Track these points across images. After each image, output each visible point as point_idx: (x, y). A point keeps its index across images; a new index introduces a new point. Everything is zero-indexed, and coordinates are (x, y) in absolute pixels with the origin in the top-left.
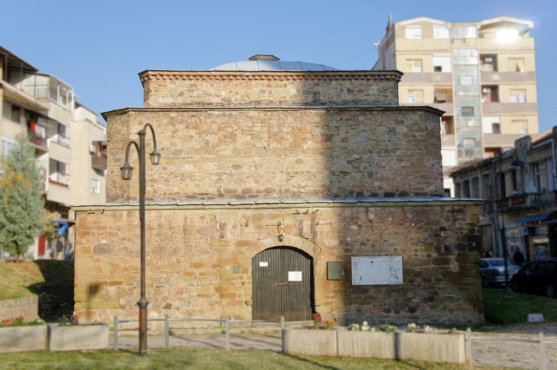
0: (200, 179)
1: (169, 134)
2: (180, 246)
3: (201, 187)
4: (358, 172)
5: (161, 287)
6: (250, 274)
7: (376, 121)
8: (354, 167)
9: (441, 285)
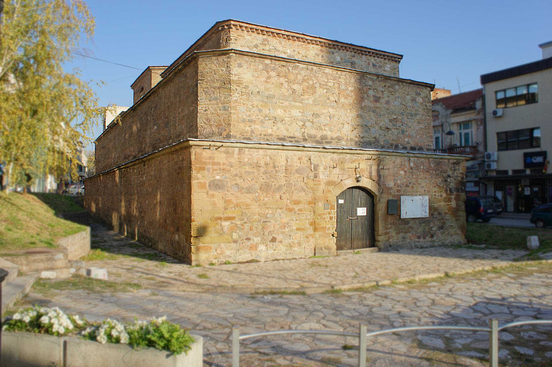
0: (289, 123)
1: (264, 79)
2: (283, 184)
3: (290, 130)
5: (267, 222)
7: (405, 90)
8: (394, 125)
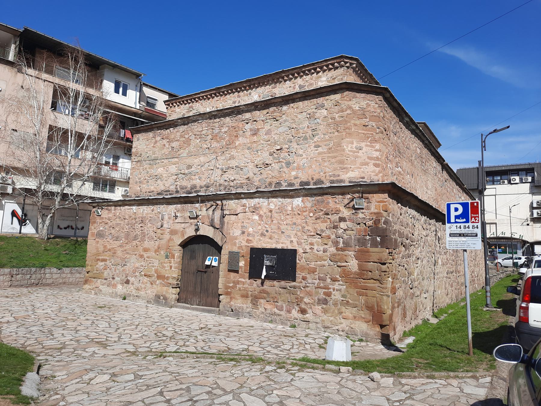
4: (277, 163)
8: (274, 158)
9: (336, 286)
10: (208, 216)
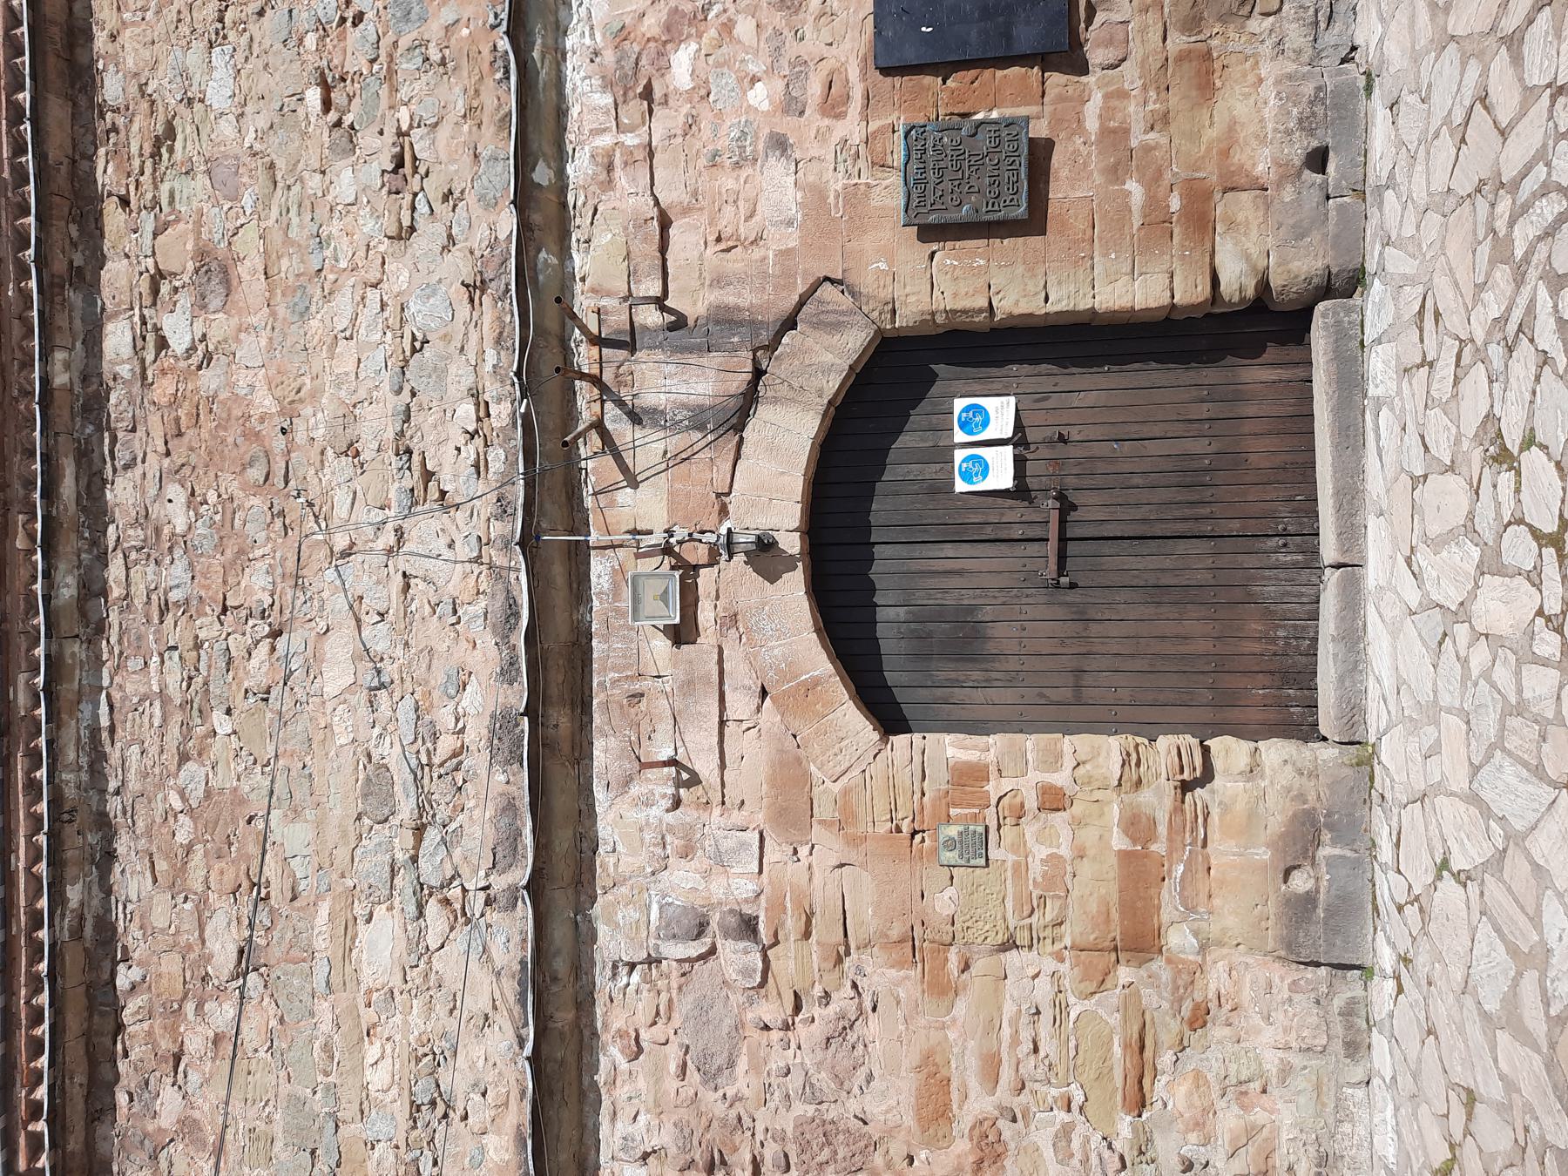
6: (991, 746)
10: (676, 460)
